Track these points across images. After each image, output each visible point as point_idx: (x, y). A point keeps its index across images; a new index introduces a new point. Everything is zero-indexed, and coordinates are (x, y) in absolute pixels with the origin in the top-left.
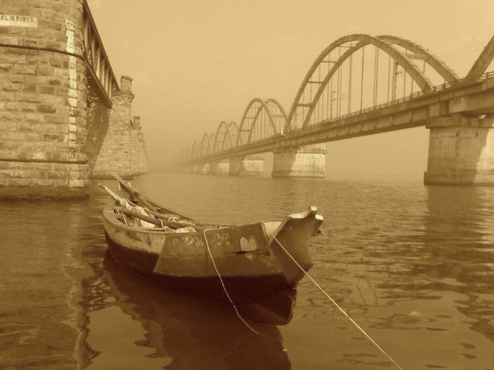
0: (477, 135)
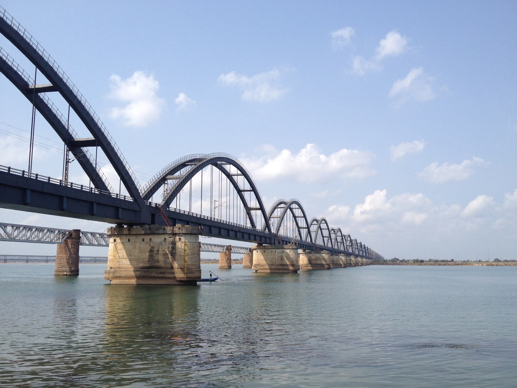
0: (129, 241)
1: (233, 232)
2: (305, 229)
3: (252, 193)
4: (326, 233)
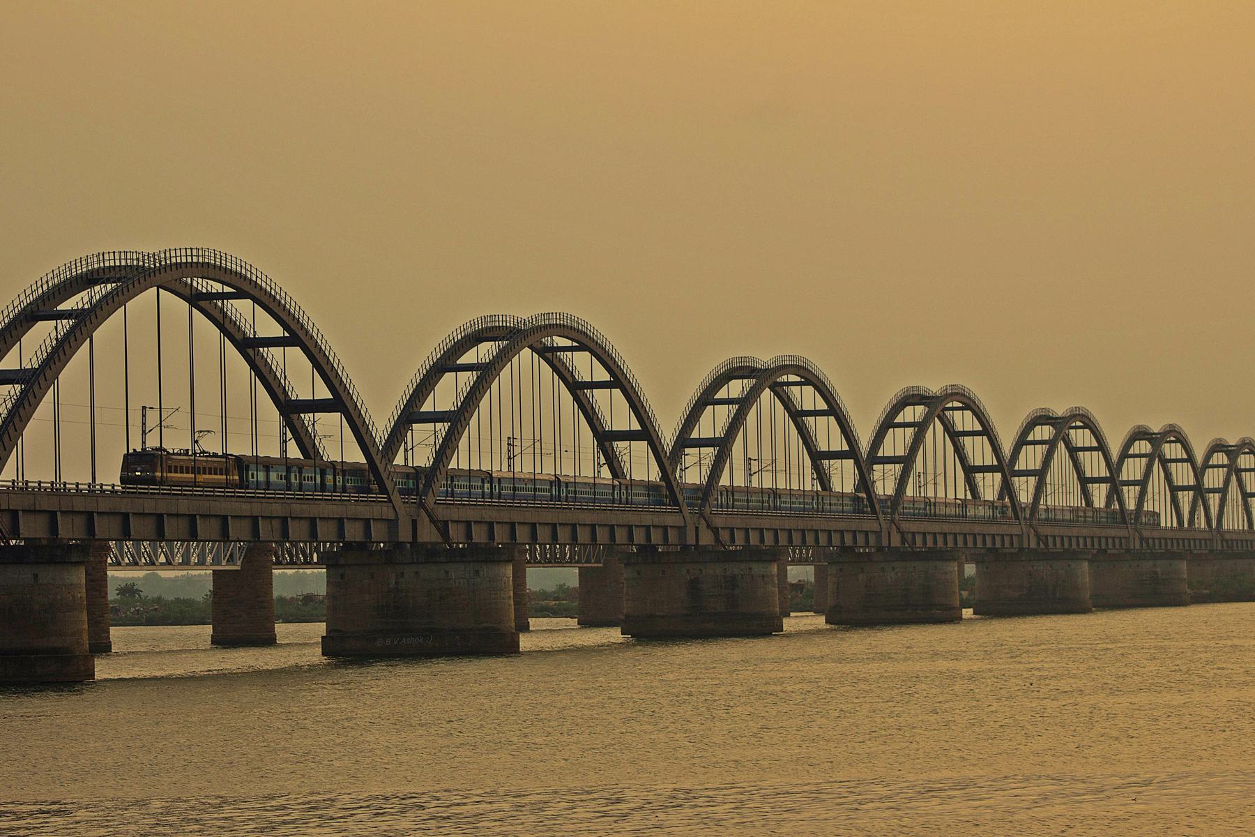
1: (643, 530)
4: (1183, 475)
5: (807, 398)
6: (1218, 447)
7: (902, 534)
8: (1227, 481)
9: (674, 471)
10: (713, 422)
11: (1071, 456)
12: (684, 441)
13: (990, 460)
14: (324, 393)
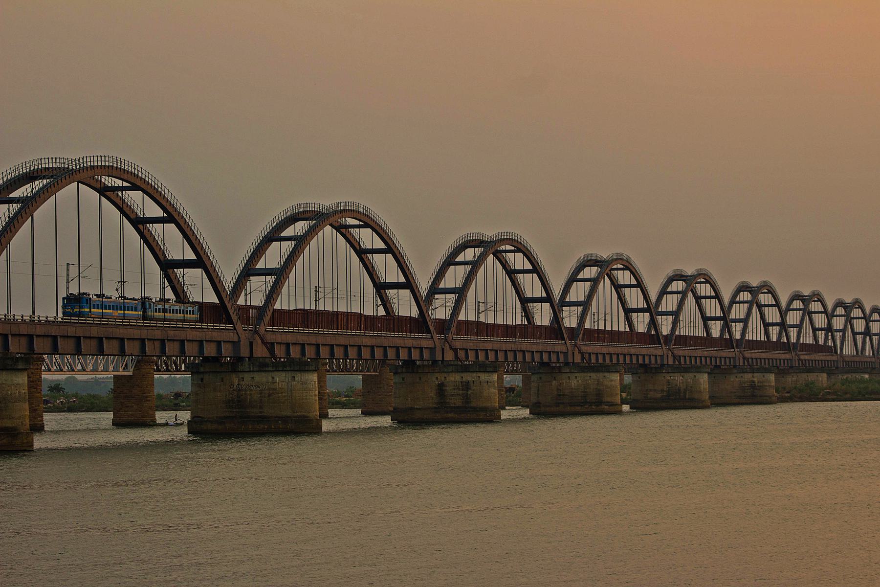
2: (718, 322)
3: (535, 275)
5: (518, 261)
6: (840, 304)
7: (582, 354)
8: (802, 320)
9: (428, 310)
10: (454, 277)
11: (697, 302)
12: (434, 290)
13: (642, 304)
14: (190, 255)
